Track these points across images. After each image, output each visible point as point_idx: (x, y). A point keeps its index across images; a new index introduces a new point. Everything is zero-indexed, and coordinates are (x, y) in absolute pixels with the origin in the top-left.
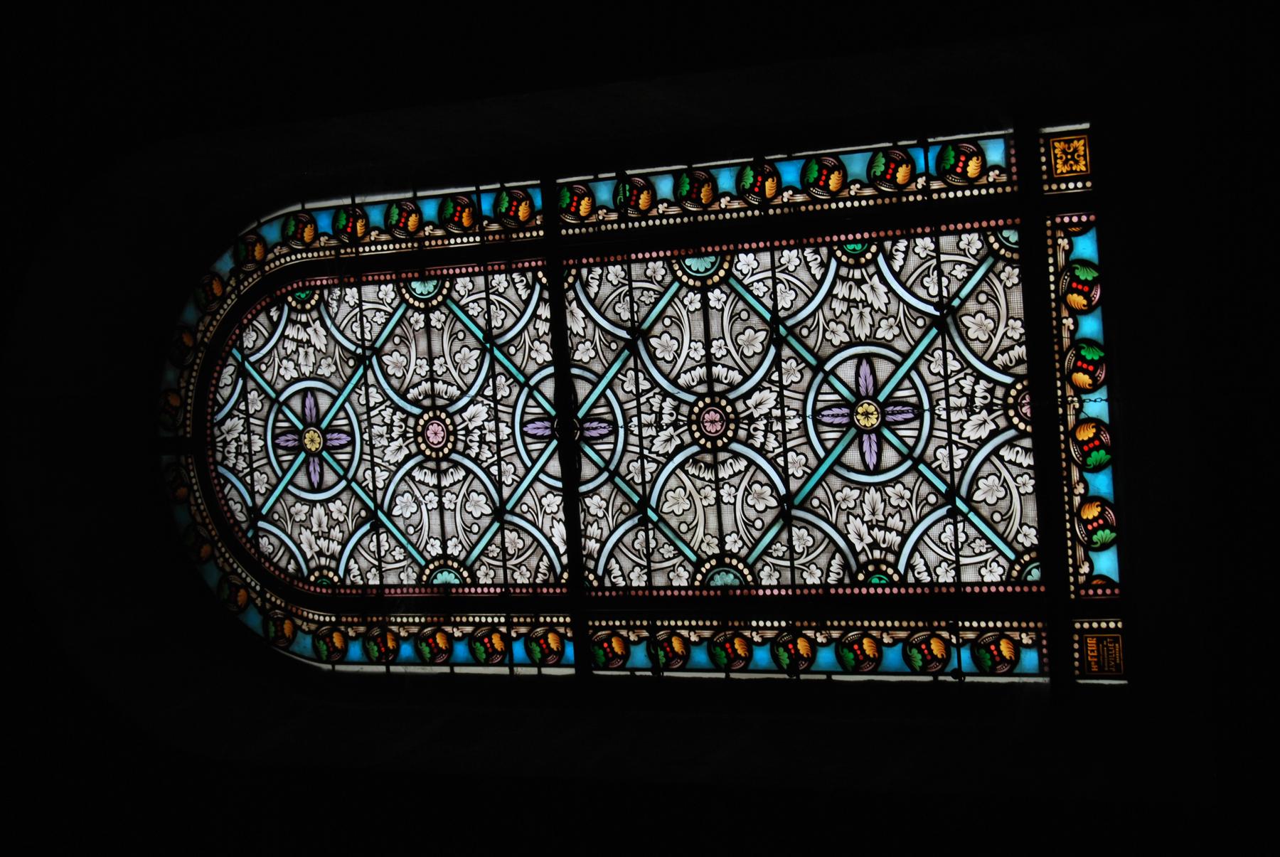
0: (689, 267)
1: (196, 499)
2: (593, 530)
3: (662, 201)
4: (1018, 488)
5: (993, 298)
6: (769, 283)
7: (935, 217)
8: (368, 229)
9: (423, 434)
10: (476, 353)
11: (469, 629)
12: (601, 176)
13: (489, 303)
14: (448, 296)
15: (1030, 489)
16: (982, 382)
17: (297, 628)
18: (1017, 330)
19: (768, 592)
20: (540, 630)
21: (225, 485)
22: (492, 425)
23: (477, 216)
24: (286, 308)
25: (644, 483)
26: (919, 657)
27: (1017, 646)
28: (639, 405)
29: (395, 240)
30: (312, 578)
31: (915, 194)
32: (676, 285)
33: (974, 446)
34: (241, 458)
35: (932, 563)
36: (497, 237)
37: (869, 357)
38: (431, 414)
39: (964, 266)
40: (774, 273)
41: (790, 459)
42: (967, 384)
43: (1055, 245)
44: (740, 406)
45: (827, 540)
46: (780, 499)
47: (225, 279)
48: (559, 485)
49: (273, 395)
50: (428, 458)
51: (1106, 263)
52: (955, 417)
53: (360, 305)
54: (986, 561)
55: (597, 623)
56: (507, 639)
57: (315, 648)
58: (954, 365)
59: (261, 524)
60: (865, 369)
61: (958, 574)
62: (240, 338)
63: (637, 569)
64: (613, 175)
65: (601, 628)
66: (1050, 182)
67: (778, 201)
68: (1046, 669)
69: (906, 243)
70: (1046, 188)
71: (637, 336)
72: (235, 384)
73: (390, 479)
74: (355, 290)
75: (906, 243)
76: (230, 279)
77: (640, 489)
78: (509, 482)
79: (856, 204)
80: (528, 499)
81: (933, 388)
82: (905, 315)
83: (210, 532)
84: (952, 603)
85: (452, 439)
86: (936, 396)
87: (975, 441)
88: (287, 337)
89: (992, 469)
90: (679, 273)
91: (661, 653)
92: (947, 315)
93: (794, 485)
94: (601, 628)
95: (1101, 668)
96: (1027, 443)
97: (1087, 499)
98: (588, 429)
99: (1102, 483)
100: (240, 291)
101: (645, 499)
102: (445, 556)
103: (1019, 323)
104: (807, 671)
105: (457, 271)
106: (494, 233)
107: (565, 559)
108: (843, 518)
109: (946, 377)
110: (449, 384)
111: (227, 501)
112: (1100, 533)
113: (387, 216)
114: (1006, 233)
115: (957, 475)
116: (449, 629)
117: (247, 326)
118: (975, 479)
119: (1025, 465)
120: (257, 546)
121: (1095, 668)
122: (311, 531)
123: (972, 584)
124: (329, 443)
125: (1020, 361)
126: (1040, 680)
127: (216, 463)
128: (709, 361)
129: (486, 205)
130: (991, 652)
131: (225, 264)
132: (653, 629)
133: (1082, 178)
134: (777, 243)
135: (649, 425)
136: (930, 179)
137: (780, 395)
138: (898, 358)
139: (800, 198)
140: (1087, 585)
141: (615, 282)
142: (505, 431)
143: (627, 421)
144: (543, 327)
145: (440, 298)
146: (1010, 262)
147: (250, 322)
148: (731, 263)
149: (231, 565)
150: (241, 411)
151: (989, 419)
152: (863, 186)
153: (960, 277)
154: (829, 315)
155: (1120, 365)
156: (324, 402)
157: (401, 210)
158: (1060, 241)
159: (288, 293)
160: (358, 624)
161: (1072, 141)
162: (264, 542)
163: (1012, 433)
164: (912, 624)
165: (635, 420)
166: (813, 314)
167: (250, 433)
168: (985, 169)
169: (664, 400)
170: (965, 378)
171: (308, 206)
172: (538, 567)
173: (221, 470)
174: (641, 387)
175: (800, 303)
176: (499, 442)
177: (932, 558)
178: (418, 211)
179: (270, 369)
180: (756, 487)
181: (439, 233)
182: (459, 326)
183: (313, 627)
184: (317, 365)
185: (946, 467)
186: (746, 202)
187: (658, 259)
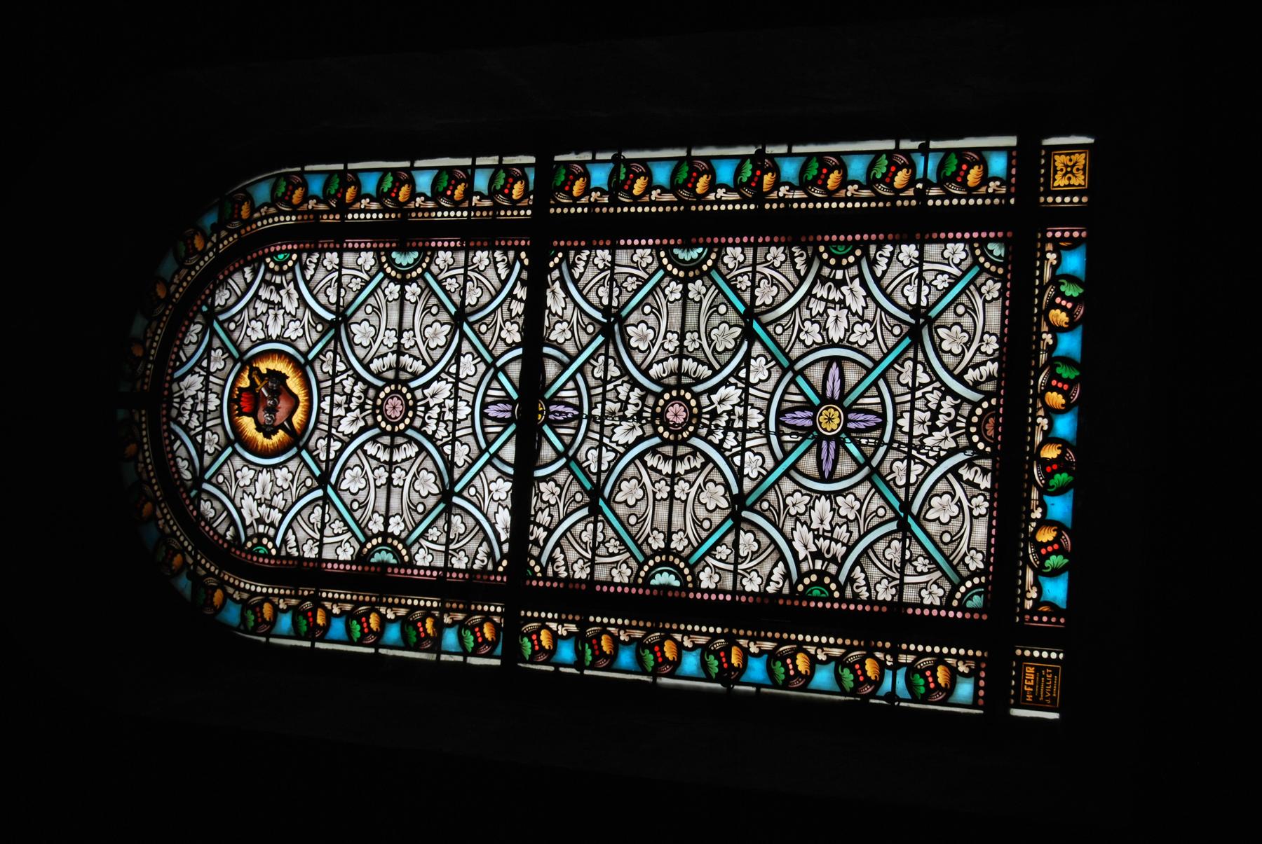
1: (145, 458)
2: (543, 518)
3: (853, 183)
6: (461, 279)
7: (919, 224)
8: (359, 197)
9: (408, 408)
10: (447, 328)
11: (402, 612)
14: (428, 269)
17: (227, 596)
18: (992, 346)
19: (706, 596)
20: (477, 618)
21: (175, 441)
23: (469, 192)
25: (908, 485)
27: (954, 673)
29: (385, 210)
30: (249, 544)
32: (661, 273)
34: (195, 416)
37: (839, 360)
38: (393, 387)
39: (946, 276)
40: (466, 271)
41: (747, 459)
45: (772, 547)
48: (510, 471)
50: (384, 432)
51: (1091, 280)
52: (336, 412)
53: (612, 269)
55: (529, 614)
56: (440, 626)
57: (244, 619)
58: (614, 371)
59: (206, 486)
60: (834, 371)
61: (320, 553)
62: (213, 295)
63: (310, 542)
65: (532, 619)
66: (1046, 194)
67: (774, 196)
68: (981, 702)
70: (1042, 199)
71: (612, 325)
72: (199, 343)
73: (340, 452)
74: (335, 254)
77: (594, 478)
78: (460, 463)
79: (850, 205)
80: (772, 496)
84: (893, 624)
85: (410, 414)
86: (324, 392)
89: (948, 488)
92: (614, 322)
94: (532, 619)
95: (1036, 698)
96: (987, 463)
97: (1044, 522)
98: (808, 418)
99: (1060, 508)
100: (218, 249)
101: (906, 505)
103: (994, 338)
104: (322, 640)
107: (506, 548)
108: (239, 494)
109: (913, 390)
110: (416, 359)
111: (174, 458)
112: (1053, 558)
113: (327, 185)
115: (603, 476)
116: (383, 610)
118: (928, 497)
119: (982, 487)
120: (197, 507)
121: (1029, 698)
122: (256, 494)
125: (990, 377)
127: (170, 418)
128: (400, 351)
130: (926, 678)
131: (210, 219)
132: (584, 625)
133: (1080, 193)
134: (472, 244)
138: (869, 364)
140: (1034, 611)
141: (907, 262)
142: (464, 411)
144: (518, 308)
145: (419, 270)
146: (994, 277)
147: (226, 278)
148: (431, 257)
149: (171, 527)
150: (740, 379)
152: (861, 187)
153: (940, 287)
155: (1095, 388)
157: (289, 183)
158: (1048, 255)
160: (291, 597)
163: (656, 440)
164: (920, 648)
165: (328, 399)
168: (985, 179)
169: (632, 390)
171: (351, 166)
174: (338, 369)
175: (486, 298)
179: (788, 332)
181: (430, 205)
182: (433, 301)
183: (245, 596)
185: (594, 469)
186: (438, 203)
187: (647, 246)
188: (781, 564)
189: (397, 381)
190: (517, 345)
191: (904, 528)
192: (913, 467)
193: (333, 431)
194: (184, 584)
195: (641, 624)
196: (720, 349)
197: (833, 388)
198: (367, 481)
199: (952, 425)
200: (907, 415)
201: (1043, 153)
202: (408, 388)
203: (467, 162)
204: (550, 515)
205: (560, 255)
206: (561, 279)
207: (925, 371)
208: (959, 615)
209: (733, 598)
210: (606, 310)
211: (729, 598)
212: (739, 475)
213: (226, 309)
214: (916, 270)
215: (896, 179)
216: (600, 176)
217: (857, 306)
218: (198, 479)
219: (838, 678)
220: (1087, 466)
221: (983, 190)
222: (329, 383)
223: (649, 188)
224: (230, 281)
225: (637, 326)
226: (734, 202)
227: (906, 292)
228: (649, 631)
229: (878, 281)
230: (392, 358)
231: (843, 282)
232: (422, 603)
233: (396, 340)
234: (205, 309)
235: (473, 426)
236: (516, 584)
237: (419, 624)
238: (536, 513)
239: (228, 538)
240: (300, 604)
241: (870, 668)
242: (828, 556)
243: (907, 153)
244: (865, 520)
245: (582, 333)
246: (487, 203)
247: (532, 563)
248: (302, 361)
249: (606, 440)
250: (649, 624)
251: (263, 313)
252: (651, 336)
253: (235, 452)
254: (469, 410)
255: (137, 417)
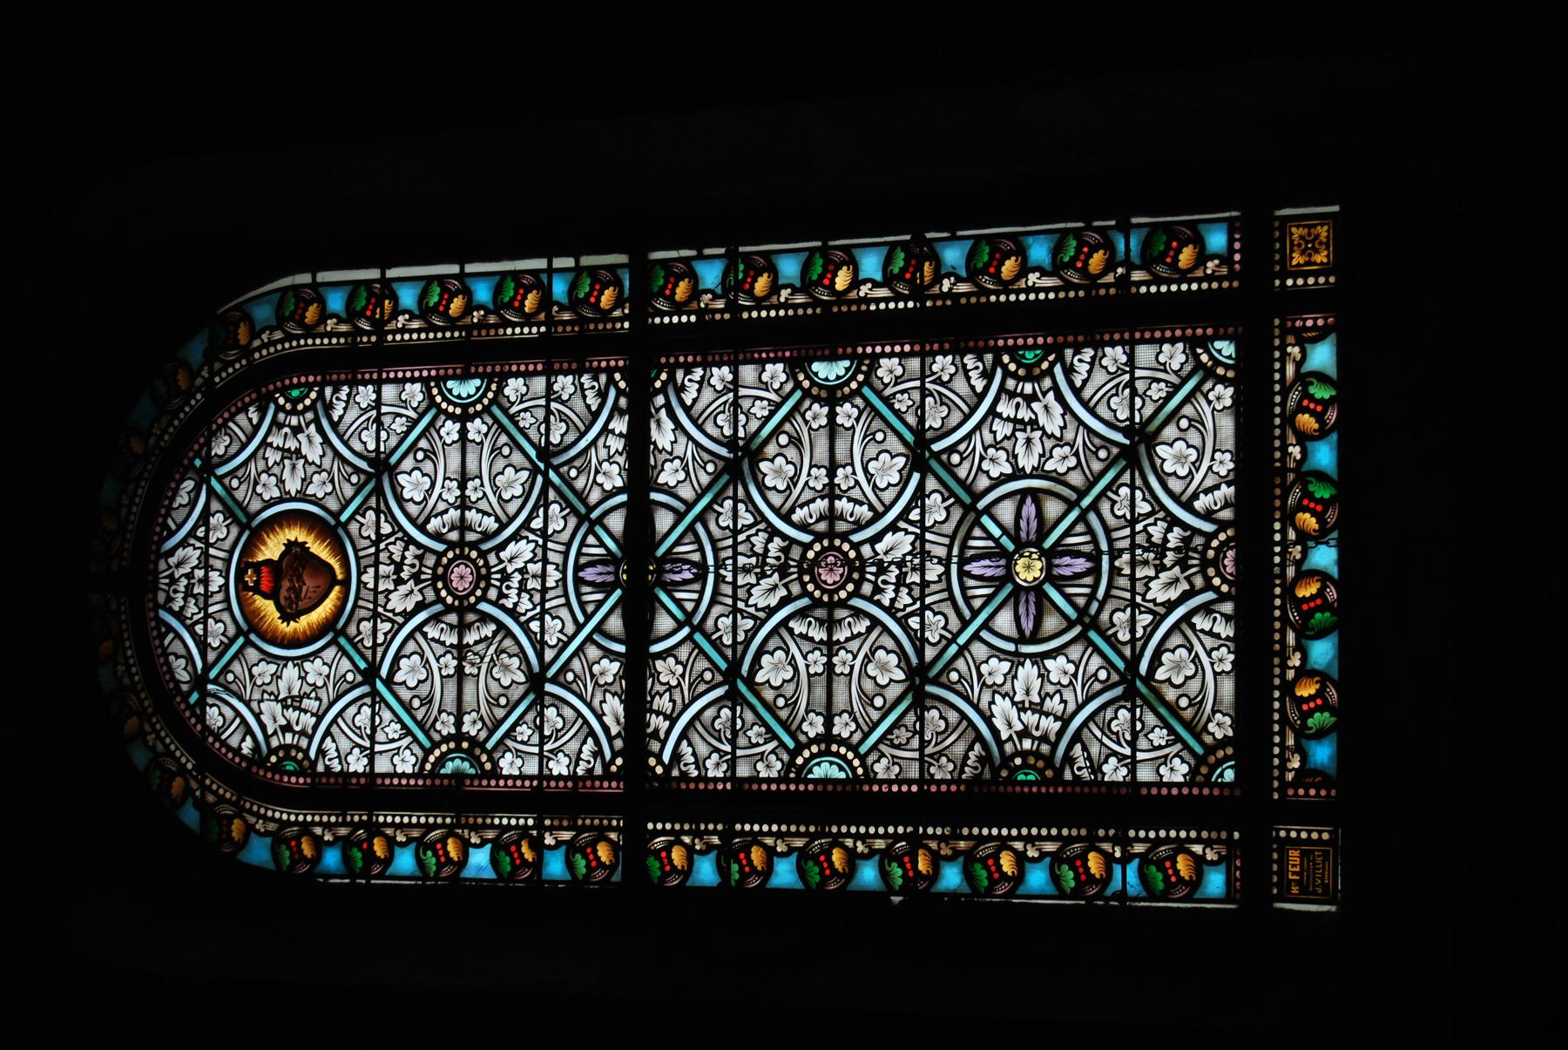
0: (450, 391)
4: (1212, 664)
5: (796, 441)
6: (916, 395)
9: (479, 578)
10: (525, 475)
12: (707, 252)
13: (924, 393)
15: (1228, 667)
16: (1176, 529)
17: (250, 829)
18: (1225, 464)
22: (535, 568)
23: (546, 301)
24: (272, 408)
26: (1071, 874)
27: (1199, 863)
28: (1133, 534)
30: (273, 759)
31: (1107, 286)
33: (762, 615)
34: (525, 596)
35: (567, 749)
36: (342, 341)
37: (1035, 494)
39: (1162, 385)
40: (923, 383)
42: (759, 541)
43: (1285, 355)
44: (866, 551)
46: (911, 672)
47: (195, 368)
49: (583, 510)
50: (817, 603)
54: (1166, 756)
58: (746, 518)
61: (371, 763)
64: (722, 251)
69: (1092, 352)
71: (739, 462)
72: (192, 504)
75: (1092, 352)
76: (201, 369)
78: (216, 644)
81: (1115, 535)
82: (694, 458)
83: (141, 701)
84: (1132, 805)
87: (762, 610)
88: (271, 445)
90: (438, 399)
91: (735, 867)
92: (1139, 442)
93: (930, 653)
96: (1228, 608)
97: (1304, 672)
98: (1058, 566)
99: (1323, 652)
101: (735, 664)
102: (459, 736)
103: (1228, 456)
104: (381, 876)
105: (1020, 342)
106: (564, 323)
107: (619, 744)
109: (735, 532)
111: (166, 654)
113: (423, 296)
114: (1218, 344)
115: (740, 648)
117: (219, 428)
118: (397, 658)
120: (202, 718)
122: (280, 698)
123: (1149, 785)
124: (1056, 571)
126: (1325, 908)
127: (157, 606)
128: (463, 504)
129: (559, 288)
135: (747, 570)
136: (1130, 267)
137: (920, 538)
139: (963, 288)
140: (1295, 784)
141: (719, 388)
142: (553, 576)
143: (719, 564)
144: (616, 444)
151: (1182, 577)
154: (988, 438)
155: (1356, 512)
156: (1053, 508)
157: (444, 290)
159: (276, 390)
161: (1315, 226)
162: (212, 712)
165: (371, 571)
166: (969, 436)
167: (208, 568)
170: (1155, 524)
172: (966, 757)
173: (164, 615)
176: (544, 590)
177: (345, 745)
178: (467, 293)
180: (881, 654)
184: (307, 481)
188: (248, 738)
189: (462, 543)
190: (619, 491)
191: (1130, 695)
192: (380, 625)
193: (1139, 599)
194: (190, 816)
195: (802, 829)
196: (882, 485)
197: (1029, 526)
198: (796, 669)
199: (416, 578)
200: (371, 571)
201: (1277, 224)
202: (851, 542)
203: (541, 264)
204: (671, 700)
205: (664, 376)
206: (668, 406)
207: (1144, 499)
208: (1206, 791)
209: (920, 788)
210: (731, 443)
211: (914, 788)
212: (919, 642)
213: (226, 459)
214: (374, 413)
215: (1181, 257)
216: (710, 275)
217: (1053, 427)
218: (199, 681)
219: (1055, 879)
220: (1355, 607)
221: (1199, 273)
222: (1127, 531)
223: (775, 288)
224: (231, 424)
225: (409, 474)
226: (887, 300)
227: (719, 422)
228: (813, 837)
229: (1077, 392)
230: (454, 514)
231: (1032, 398)
232: (513, 822)
233: (458, 493)
234: (198, 463)
235: (566, 595)
236: (638, 789)
237: (1168, 864)
238: (653, 698)
239: (245, 751)
240: (976, 847)
241: (1094, 863)
242: (1037, 734)
243: (1102, 231)
244: (1083, 686)
245: (701, 473)
246: (344, 328)
247: (652, 762)
248: (333, 522)
249: (741, 605)
250: (812, 829)
251: (1006, 437)
252: (1194, 457)
253: (248, 643)
254: (558, 576)
255: (113, 606)
